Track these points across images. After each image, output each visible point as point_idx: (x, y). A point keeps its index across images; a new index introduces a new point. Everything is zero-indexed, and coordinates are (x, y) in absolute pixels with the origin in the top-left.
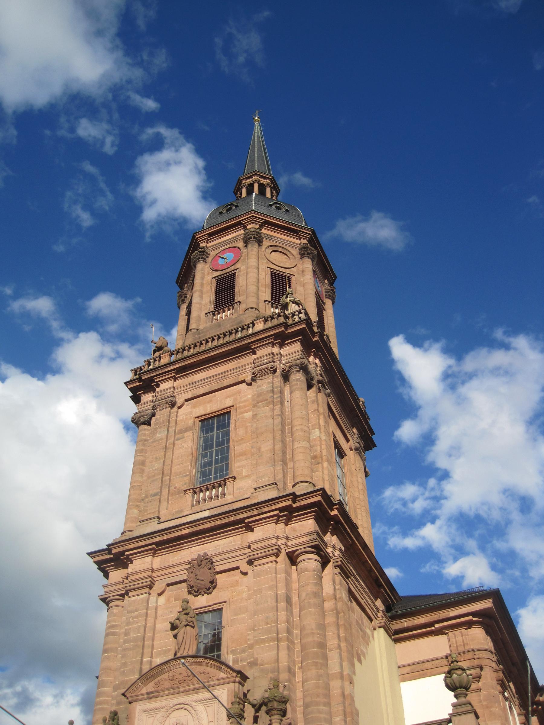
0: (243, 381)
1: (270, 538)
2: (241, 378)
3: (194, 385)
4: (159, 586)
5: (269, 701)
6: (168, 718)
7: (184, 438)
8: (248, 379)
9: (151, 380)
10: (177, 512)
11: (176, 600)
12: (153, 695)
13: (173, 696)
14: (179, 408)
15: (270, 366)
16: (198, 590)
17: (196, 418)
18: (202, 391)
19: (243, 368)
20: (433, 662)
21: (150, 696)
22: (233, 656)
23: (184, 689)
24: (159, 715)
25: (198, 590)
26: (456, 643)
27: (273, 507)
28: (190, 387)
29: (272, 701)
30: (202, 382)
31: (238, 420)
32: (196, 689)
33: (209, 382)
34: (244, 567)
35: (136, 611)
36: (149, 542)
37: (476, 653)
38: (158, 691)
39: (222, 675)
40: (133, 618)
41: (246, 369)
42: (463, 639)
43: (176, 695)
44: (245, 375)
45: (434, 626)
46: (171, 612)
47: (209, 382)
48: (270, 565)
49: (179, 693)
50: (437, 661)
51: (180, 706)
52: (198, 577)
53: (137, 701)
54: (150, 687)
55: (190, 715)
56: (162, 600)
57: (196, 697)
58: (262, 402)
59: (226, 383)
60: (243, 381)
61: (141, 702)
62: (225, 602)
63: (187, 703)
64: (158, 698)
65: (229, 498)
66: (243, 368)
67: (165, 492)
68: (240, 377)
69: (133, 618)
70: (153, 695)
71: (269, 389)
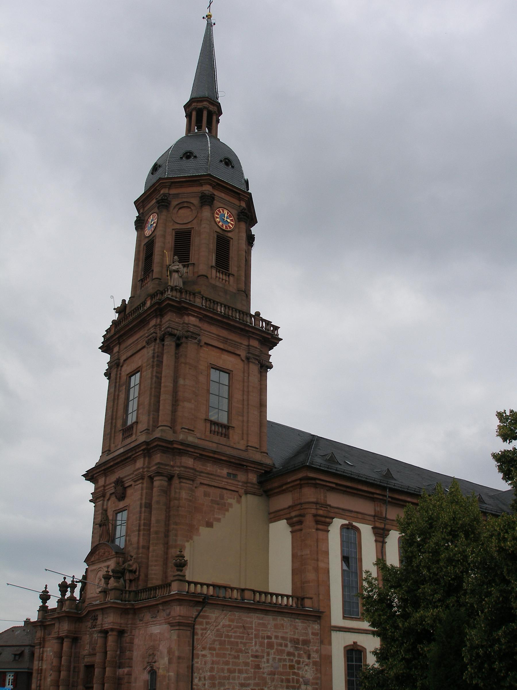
41: (227, 342)
49: (100, 562)
60: (239, 355)
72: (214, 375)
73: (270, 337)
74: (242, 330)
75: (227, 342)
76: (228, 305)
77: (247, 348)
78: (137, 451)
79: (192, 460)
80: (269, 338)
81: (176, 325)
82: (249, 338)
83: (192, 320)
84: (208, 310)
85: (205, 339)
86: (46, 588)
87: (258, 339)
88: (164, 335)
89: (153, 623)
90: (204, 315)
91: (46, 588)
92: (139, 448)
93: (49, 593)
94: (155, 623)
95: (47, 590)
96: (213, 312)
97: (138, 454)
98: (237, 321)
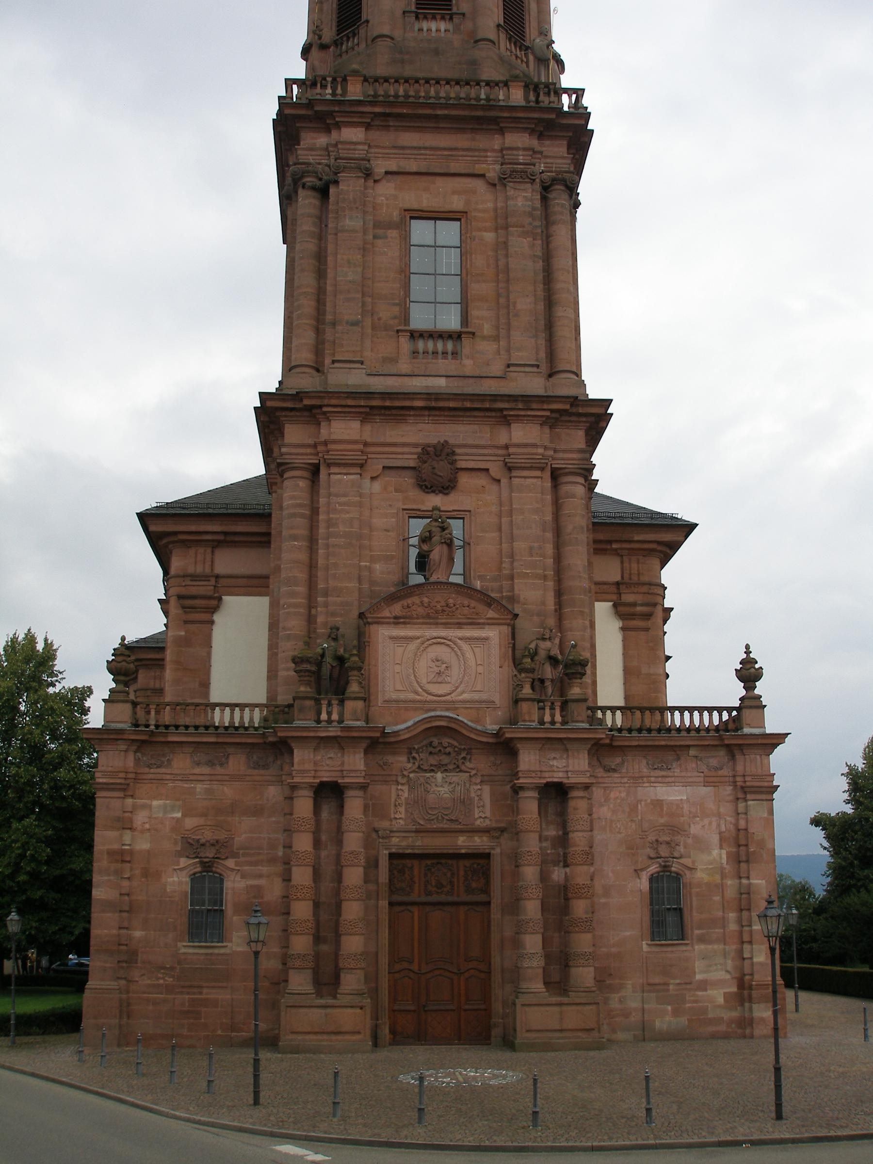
0: (482, 176)
1: (535, 446)
2: (479, 168)
3: (401, 152)
4: (376, 467)
5: (573, 664)
6: (425, 652)
7: (386, 237)
8: (491, 175)
9: (331, 114)
10: (385, 360)
11: (396, 491)
12: (402, 620)
13: (429, 626)
14: (375, 181)
15: (529, 171)
16: (431, 487)
17: (405, 210)
18: (413, 167)
19: (482, 154)
20: (601, 586)
21: (397, 621)
22: (481, 582)
23: (443, 621)
24: (413, 646)
25: (431, 487)
26: (630, 571)
27: (545, 407)
28: (394, 151)
29: (577, 664)
30: (416, 152)
31: (474, 240)
32: (459, 623)
33: (426, 155)
34: (496, 470)
35: (345, 495)
36: (362, 403)
37: (653, 587)
38: (411, 617)
39: (491, 614)
40: (340, 504)
41: (487, 157)
42: (638, 567)
43: (432, 626)
44: (485, 165)
45: (611, 545)
46: (390, 506)
47: (426, 155)
48: (534, 480)
49: (437, 624)
50: (605, 586)
51: (439, 641)
52: (436, 471)
53: (378, 623)
54: (397, 609)
55: (453, 654)
56: (377, 486)
57: (460, 633)
58: (516, 227)
59: (455, 167)
60: (482, 176)
61: (384, 625)
62: (470, 511)
63: (450, 638)
64: (408, 626)
65: (468, 365)
66: (482, 154)
67: (368, 322)
68: (477, 166)
69: (340, 504)
70: (402, 620)
71: (528, 209)
72: (420, 231)
73: (553, 116)
74: (479, 120)
75: (487, 157)
76: (433, 76)
77: (500, 154)
78: (545, 407)
79: (359, 423)
80: (551, 120)
81: (317, 155)
82: (502, 131)
83: (352, 134)
84: (465, 104)
85: (380, 166)
86: (748, 652)
87: (525, 129)
88: (554, 181)
89: (664, 779)
90: (372, 115)
91: (748, 652)
92: (549, 403)
93: (756, 662)
94: (670, 780)
95: (752, 655)
96: (469, 105)
97: (529, 413)
98: (531, 107)
